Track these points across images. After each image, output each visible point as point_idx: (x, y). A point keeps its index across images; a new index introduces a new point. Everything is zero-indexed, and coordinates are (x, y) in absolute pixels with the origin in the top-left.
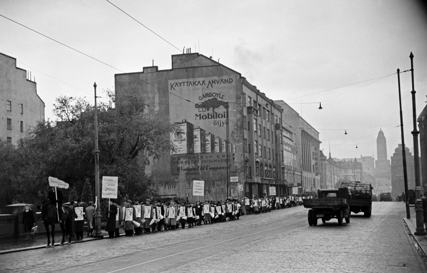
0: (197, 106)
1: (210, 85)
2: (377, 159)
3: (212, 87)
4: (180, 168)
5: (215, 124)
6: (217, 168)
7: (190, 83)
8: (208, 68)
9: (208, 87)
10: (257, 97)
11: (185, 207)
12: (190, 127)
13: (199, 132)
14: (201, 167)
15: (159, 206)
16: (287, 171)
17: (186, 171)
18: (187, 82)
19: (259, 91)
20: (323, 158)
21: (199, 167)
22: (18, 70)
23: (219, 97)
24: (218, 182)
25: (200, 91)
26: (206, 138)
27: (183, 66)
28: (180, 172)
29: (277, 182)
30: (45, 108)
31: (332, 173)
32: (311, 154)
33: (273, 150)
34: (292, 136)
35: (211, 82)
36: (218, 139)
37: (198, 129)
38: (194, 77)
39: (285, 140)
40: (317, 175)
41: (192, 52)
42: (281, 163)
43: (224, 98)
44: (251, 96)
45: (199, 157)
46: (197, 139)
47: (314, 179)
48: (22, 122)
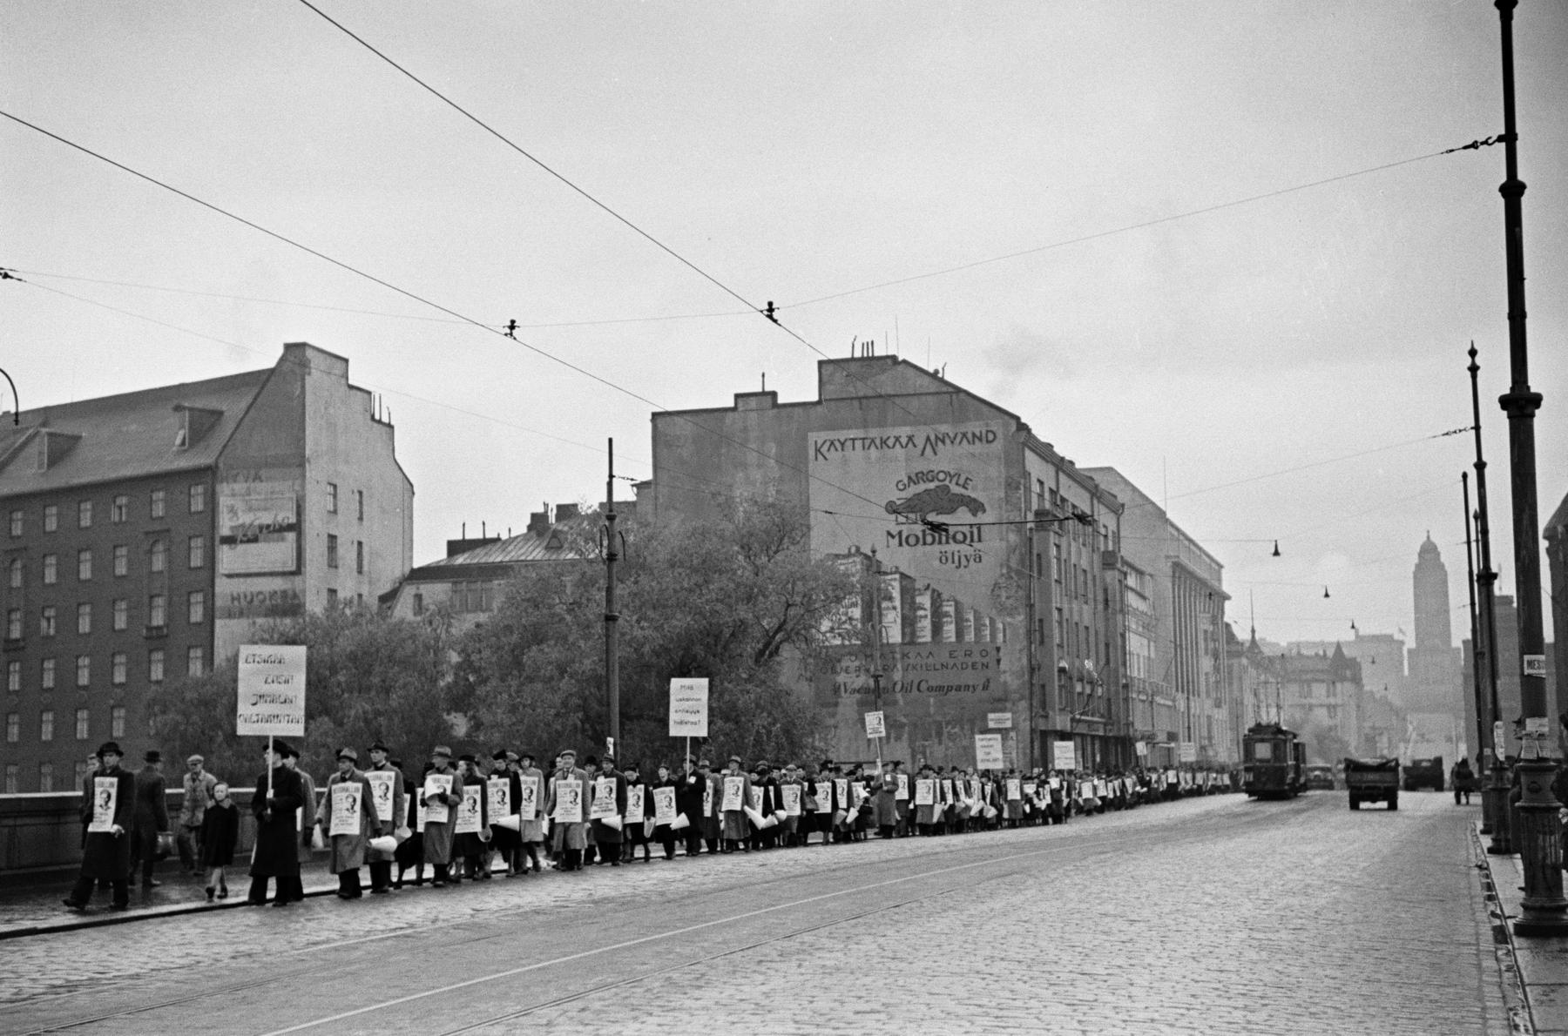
0: (892, 509)
1: (929, 448)
2: (1413, 645)
3: (935, 453)
4: (842, 688)
5: (944, 561)
6: (950, 688)
7: (873, 441)
8: (924, 398)
10: (1092, 505)
11: (614, 779)
13: (896, 584)
14: (903, 684)
15: (501, 774)
17: (858, 696)
18: (864, 439)
20: (1234, 648)
21: (895, 684)
22: (354, 391)
23: (957, 484)
24: (953, 728)
25: (900, 464)
26: (919, 600)
27: (851, 391)
28: (841, 697)
29: (1109, 727)
34: (1142, 584)
35: (933, 438)
36: (953, 603)
37: (895, 573)
38: (881, 424)
40: (1218, 705)
41: (876, 354)
42: (1121, 670)
43: (969, 487)
44: (1043, 479)
45: (898, 656)
47: (1209, 717)
48: (360, 544)
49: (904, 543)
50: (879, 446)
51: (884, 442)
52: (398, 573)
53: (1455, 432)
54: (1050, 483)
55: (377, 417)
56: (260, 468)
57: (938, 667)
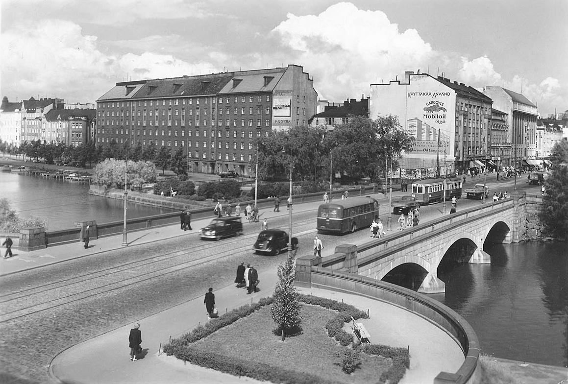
52: (313, 114)
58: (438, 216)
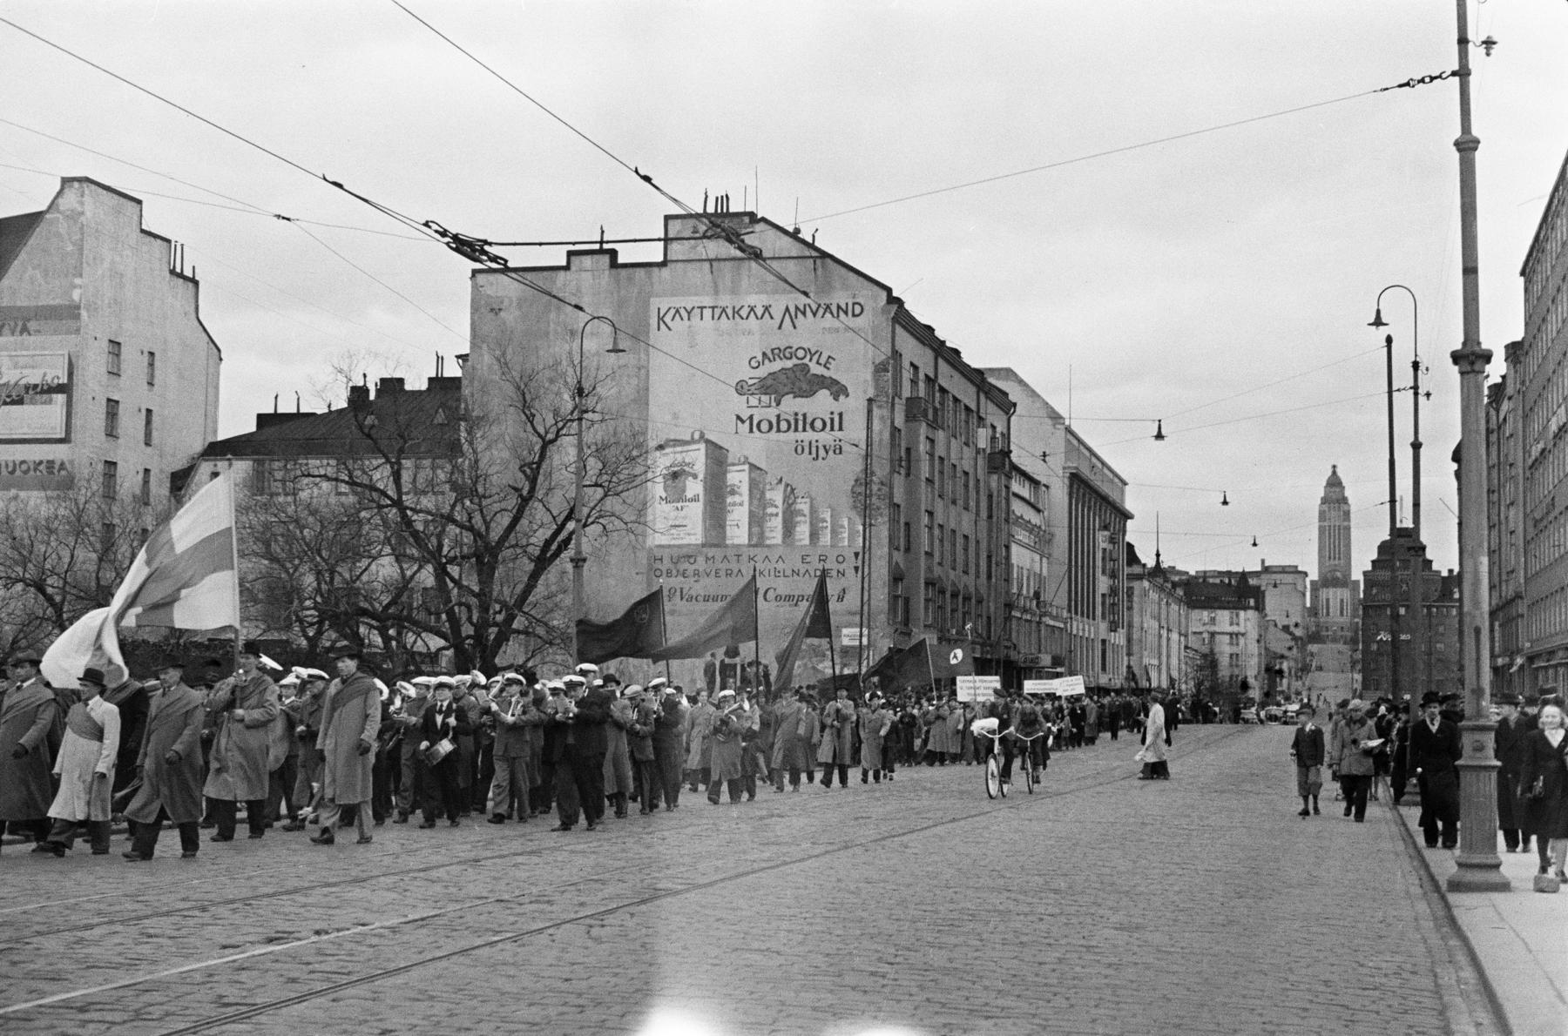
0: (741, 388)
7: (724, 310)
9: (780, 327)
12: (718, 458)
13: (745, 477)
16: (1019, 615)
18: (713, 308)
19: (943, 343)
23: (818, 363)
25: (753, 338)
26: (768, 495)
30: (223, 366)
31: (1164, 623)
32: (1099, 555)
33: (978, 542)
35: (792, 310)
36: (808, 500)
39: (1018, 508)
40: (1113, 627)
44: (916, 363)
46: (737, 499)
47: (1104, 641)
48: (149, 411)
49: (755, 429)
50: (730, 316)
51: (736, 312)
53: (1422, 81)
54: (926, 368)
55: (178, 270)
56: (29, 320)
57: (789, 572)
58: (1174, 661)
